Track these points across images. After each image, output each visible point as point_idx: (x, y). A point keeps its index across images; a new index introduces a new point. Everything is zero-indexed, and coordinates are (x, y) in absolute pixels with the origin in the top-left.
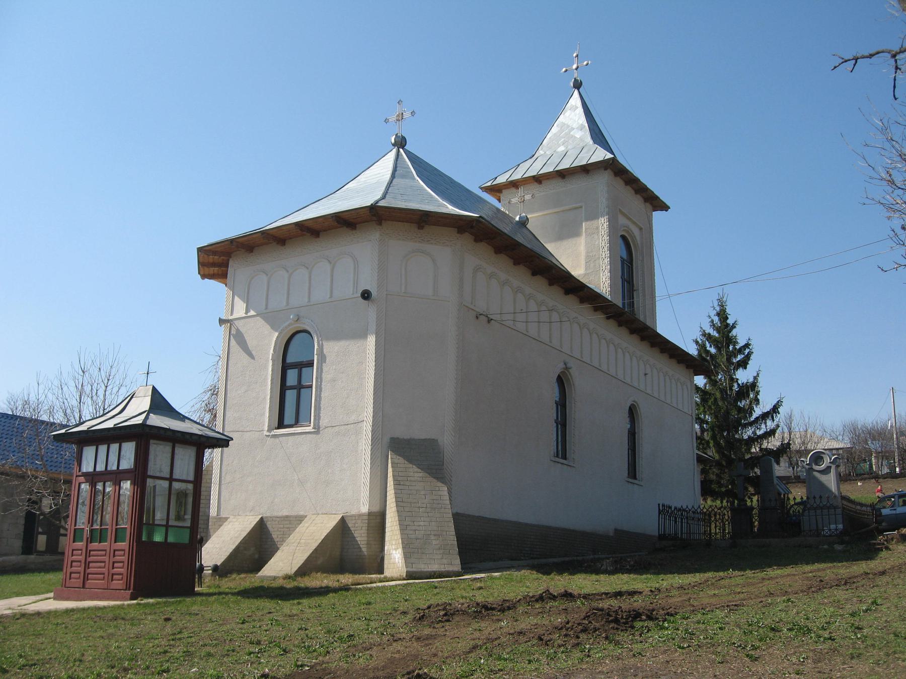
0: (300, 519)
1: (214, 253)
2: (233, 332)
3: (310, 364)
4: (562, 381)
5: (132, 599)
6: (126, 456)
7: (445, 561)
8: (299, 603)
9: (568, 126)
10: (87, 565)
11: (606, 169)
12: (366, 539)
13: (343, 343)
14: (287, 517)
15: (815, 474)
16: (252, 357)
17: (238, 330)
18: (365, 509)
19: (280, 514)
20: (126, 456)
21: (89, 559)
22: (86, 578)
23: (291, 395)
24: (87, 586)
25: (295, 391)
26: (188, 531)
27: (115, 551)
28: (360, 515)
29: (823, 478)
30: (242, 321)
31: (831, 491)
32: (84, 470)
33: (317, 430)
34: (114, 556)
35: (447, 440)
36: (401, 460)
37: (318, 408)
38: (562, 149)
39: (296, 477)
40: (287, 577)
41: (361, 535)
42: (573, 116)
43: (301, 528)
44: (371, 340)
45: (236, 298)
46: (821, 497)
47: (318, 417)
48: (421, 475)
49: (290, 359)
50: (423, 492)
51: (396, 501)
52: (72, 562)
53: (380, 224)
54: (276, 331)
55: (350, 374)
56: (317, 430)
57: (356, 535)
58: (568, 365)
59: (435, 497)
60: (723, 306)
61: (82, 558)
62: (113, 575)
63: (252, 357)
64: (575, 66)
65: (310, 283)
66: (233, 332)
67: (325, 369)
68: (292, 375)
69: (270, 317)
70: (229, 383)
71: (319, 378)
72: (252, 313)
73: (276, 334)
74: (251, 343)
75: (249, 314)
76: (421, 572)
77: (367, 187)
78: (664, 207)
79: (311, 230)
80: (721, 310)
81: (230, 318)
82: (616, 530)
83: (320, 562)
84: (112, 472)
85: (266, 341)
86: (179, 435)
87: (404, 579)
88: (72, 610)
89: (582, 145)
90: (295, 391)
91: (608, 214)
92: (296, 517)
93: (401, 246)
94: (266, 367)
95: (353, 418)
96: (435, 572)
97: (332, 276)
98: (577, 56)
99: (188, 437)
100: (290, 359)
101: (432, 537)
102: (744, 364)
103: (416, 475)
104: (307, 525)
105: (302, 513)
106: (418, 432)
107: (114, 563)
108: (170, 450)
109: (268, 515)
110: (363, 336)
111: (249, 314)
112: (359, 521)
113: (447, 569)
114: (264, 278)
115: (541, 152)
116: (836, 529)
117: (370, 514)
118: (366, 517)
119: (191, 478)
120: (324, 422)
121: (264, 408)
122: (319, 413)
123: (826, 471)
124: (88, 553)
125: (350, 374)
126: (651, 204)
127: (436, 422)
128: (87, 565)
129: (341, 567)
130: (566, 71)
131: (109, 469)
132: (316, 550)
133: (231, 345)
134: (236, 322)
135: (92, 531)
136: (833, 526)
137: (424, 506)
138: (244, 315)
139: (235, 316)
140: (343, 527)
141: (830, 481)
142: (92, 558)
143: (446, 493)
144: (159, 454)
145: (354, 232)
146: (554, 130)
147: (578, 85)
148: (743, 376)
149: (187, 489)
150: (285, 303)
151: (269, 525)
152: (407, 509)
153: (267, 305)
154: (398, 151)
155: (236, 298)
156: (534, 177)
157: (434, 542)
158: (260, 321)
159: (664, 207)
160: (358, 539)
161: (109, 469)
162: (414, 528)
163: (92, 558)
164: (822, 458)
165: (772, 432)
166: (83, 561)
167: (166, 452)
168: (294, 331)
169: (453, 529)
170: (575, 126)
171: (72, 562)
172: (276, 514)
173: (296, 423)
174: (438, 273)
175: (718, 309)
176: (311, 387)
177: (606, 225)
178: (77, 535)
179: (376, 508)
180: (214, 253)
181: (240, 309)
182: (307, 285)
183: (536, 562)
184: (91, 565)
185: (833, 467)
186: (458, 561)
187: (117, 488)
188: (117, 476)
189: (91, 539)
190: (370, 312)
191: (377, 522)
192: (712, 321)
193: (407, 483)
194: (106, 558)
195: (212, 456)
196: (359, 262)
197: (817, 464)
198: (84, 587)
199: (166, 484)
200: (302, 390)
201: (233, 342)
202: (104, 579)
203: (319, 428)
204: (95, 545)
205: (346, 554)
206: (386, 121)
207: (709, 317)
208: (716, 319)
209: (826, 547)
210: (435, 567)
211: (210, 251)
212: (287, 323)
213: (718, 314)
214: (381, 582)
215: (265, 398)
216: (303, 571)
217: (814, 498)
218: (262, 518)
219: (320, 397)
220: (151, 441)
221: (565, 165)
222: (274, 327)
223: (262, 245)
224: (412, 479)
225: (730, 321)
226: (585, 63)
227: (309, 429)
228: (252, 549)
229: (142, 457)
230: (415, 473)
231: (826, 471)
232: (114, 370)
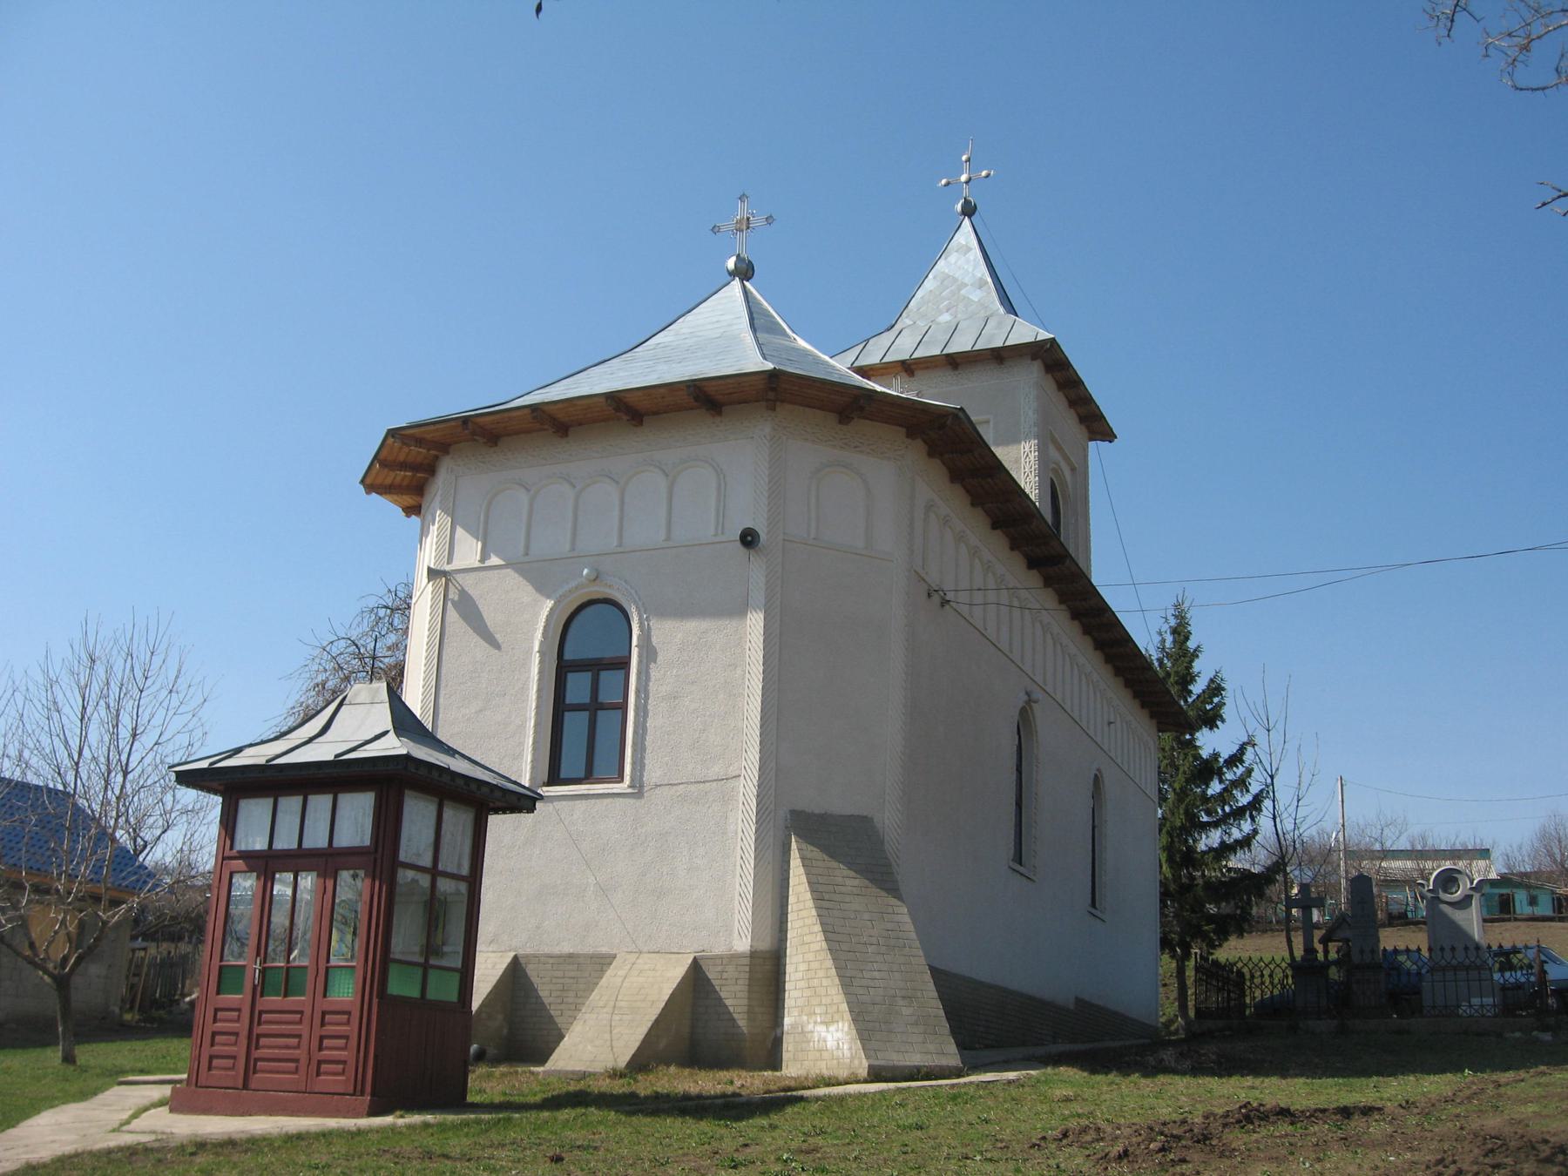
0: (602, 962)
1: (419, 441)
2: (453, 594)
3: (624, 664)
4: (1024, 724)
5: (374, 1112)
6: (354, 819)
7: (931, 1047)
8: (773, 1127)
9: (955, 280)
10: (253, 1040)
11: (1034, 358)
12: (745, 1002)
13: (692, 625)
14: (571, 956)
15: (1445, 908)
16: (495, 645)
17: (463, 593)
18: (743, 944)
19: (556, 950)
20: (354, 819)
21: (258, 1030)
22: (250, 1069)
23: (575, 724)
24: (253, 1086)
25: (585, 715)
26: (457, 976)
27: (324, 1014)
28: (734, 957)
29: (1458, 916)
30: (473, 575)
31: (1471, 938)
32: (241, 845)
33: (638, 789)
34: (323, 1024)
35: (889, 819)
36: (815, 853)
37: (640, 747)
38: (945, 318)
39: (591, 880)
40: (615, 1074)
41: (735, 996)
42: (962, 260)
43: (612, 976)
44: (755, 622)
45: (460, 531)
46: (1453, 949)
47: (639, 764)
48: (856, 882)
49: (568, 656)
50: (866, 916)
51: (824, 931)
52: (214, 1034)
53: (774, 409)
54: (548, 597)
55: (707, 689)
56: (638, 789)
57: (723, 995)
58: (1034, 696)
59: (890, 926)
60: (1183, 618)
61: (242, 1027)
62: (320, 1063)
63: (495, 645)
64: (964, 178)
65: (622, 510)
66: (453, 594)
67: (654, 674)
68: (578, 687)
69: (537, 572)
70: (442, 692)
71: (643, 690)
72: (495, 560)
73: (550, 604)
74: (491, 617)
75: (488, 563)
76: (894, 1068)
77: (715, 336)
78: (1109, 436)
79: (630, 411)
80: (1179, 625)
81: (448, 568)
82: (1078, 1001)
83: (662, 1044)
84: (315, 853)
85: (528, 619)
86: (461, 782)
87: (866, 1081)
88: (300, 1137)
89: (983, 314)
90: (585, 715)
91: (1037, 437)
92: (592, 957)
93: (809, 450)
94: (525, 664)
95: (716, 770)
96: (918, 1069)
97: (486, 523)
98: (968, 160)
99: (473, 787)
100: (568, 656)
101: (901, 1002)
102: (1212, 719)
103: (848, 882)
104: (622, 973)
105: (604, 950)
106: (837, 801)
107: (322, 1038)
108: (435, 813)
109: (529, 951)
110: (739, 610)
111: (488, 563)
112: (731, 969)
113: (937, 1063)
114: (523, 498)
115: (905, 321)
116: (1482, 1006)
117: (753, 955)
118: (747, 961)
119: (465, 871)
120: (652, 774)
121: (521, 744)
122: (643, 758)
123: (1465, 903)
124: (256, 1017)
125: (707, 689)
126: (1088, 427)
127: (871, 787)
128: (253, 1040)
129: (696, 1056)
130: (948, 184)
131: (307, 844)
132: (657, 1021)
133: (448, 619)
134: (459, 577)
135: (263, 972)
136: (1475, 1001)
137: (874, 940)
138: (478, 564)
139: (457, 564)
140: (697, 980)
141: (1472, 921)
142: (264, 1028)
143: (907, 919)
144: (418, 816)
145: (718, 419)
146: (930, 284)
147: (969, 210)
148: (1210, 742)
149: (458, 893)
150: (568, 547)
151: (532, 971)
152: (844, 947)
153: (527, 547)
154: (744, 287)
155: (460, 531)
156: (903, 362)
157: (905, 1011)
158: (512, 578)
159: (1109, 436)
160: (727, 1002)
161: (335, 844)
162: (864, 982)
163: (264, 1028)
164: (1456, 880)
165: (1246, 842)
166: (245, 1033)
167: (414, 813)
168: (585, 599)
169: (931, 986)
170: (966, 280)
171: (214, 1034)
172: (546, 950)
173: (588, 777)
174: (878, 504)
175: (1173, 622)
176: (623, 708)
177: (1033, 456)
178: (227, 978)
179: (765, 944)
180: (419, 441)
181: (468, 551)
182: (616, 513)
183: (1040, 1051)
184: (263, 1041)
185: (1476, 896)
186: (952, 1048)
187: (330, 883)
188: (328, 861)
189: (261, 989)
190: (756, 571)
191: (768, 971)
192: (1163, 641)
193: (837, 897)
194: (303, 1029)
195: (499, 826)
196: (732, 476)
197: (1445, 891)
198: (245, 1087)
199: (425, 881)
200: (600, 713)
201: (452, 614)
202: (296, 1071)
203: (642, 786)
204: (273, 1000)
205: (714, 1032)
206: (715, 230)
207: (1160, 633)
208: (1169, 639)
209: (1518, 1034)
210: (915, 1059)
211: (411, 437)
212: (573, 584)
213: (1174, 631)
214: (828, 1085)
215: (523, 726)
216: (641, 1062)
217: (1453, 949)
218: (516, 958)
219: (645, 729)
220: (407, 793)
221: (962, 344)
222: (542, 588)
223: (528, 431)
224: (843, 889)
225: (1191, 644)
226: (984, 173)
227: (623, 788)
228: (500, 1017)
229: (387, 823)
230: (847, 879)
231: (1465, 903)
232: (157, 660)
